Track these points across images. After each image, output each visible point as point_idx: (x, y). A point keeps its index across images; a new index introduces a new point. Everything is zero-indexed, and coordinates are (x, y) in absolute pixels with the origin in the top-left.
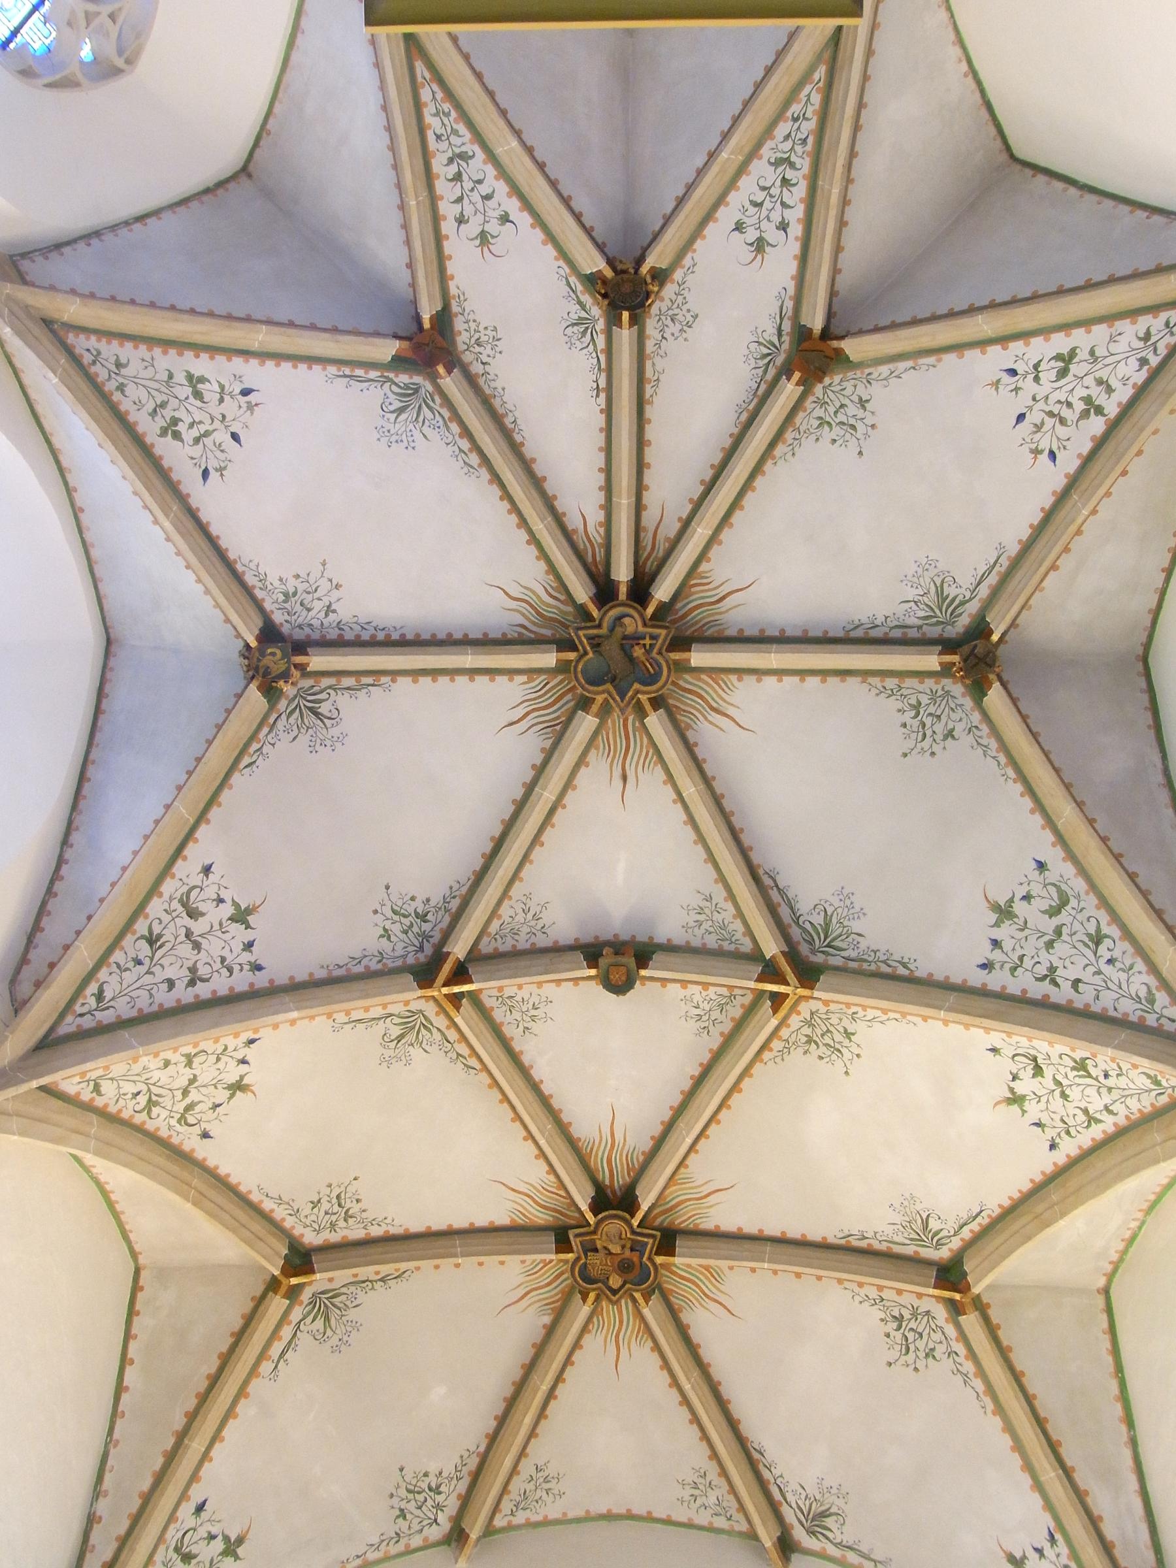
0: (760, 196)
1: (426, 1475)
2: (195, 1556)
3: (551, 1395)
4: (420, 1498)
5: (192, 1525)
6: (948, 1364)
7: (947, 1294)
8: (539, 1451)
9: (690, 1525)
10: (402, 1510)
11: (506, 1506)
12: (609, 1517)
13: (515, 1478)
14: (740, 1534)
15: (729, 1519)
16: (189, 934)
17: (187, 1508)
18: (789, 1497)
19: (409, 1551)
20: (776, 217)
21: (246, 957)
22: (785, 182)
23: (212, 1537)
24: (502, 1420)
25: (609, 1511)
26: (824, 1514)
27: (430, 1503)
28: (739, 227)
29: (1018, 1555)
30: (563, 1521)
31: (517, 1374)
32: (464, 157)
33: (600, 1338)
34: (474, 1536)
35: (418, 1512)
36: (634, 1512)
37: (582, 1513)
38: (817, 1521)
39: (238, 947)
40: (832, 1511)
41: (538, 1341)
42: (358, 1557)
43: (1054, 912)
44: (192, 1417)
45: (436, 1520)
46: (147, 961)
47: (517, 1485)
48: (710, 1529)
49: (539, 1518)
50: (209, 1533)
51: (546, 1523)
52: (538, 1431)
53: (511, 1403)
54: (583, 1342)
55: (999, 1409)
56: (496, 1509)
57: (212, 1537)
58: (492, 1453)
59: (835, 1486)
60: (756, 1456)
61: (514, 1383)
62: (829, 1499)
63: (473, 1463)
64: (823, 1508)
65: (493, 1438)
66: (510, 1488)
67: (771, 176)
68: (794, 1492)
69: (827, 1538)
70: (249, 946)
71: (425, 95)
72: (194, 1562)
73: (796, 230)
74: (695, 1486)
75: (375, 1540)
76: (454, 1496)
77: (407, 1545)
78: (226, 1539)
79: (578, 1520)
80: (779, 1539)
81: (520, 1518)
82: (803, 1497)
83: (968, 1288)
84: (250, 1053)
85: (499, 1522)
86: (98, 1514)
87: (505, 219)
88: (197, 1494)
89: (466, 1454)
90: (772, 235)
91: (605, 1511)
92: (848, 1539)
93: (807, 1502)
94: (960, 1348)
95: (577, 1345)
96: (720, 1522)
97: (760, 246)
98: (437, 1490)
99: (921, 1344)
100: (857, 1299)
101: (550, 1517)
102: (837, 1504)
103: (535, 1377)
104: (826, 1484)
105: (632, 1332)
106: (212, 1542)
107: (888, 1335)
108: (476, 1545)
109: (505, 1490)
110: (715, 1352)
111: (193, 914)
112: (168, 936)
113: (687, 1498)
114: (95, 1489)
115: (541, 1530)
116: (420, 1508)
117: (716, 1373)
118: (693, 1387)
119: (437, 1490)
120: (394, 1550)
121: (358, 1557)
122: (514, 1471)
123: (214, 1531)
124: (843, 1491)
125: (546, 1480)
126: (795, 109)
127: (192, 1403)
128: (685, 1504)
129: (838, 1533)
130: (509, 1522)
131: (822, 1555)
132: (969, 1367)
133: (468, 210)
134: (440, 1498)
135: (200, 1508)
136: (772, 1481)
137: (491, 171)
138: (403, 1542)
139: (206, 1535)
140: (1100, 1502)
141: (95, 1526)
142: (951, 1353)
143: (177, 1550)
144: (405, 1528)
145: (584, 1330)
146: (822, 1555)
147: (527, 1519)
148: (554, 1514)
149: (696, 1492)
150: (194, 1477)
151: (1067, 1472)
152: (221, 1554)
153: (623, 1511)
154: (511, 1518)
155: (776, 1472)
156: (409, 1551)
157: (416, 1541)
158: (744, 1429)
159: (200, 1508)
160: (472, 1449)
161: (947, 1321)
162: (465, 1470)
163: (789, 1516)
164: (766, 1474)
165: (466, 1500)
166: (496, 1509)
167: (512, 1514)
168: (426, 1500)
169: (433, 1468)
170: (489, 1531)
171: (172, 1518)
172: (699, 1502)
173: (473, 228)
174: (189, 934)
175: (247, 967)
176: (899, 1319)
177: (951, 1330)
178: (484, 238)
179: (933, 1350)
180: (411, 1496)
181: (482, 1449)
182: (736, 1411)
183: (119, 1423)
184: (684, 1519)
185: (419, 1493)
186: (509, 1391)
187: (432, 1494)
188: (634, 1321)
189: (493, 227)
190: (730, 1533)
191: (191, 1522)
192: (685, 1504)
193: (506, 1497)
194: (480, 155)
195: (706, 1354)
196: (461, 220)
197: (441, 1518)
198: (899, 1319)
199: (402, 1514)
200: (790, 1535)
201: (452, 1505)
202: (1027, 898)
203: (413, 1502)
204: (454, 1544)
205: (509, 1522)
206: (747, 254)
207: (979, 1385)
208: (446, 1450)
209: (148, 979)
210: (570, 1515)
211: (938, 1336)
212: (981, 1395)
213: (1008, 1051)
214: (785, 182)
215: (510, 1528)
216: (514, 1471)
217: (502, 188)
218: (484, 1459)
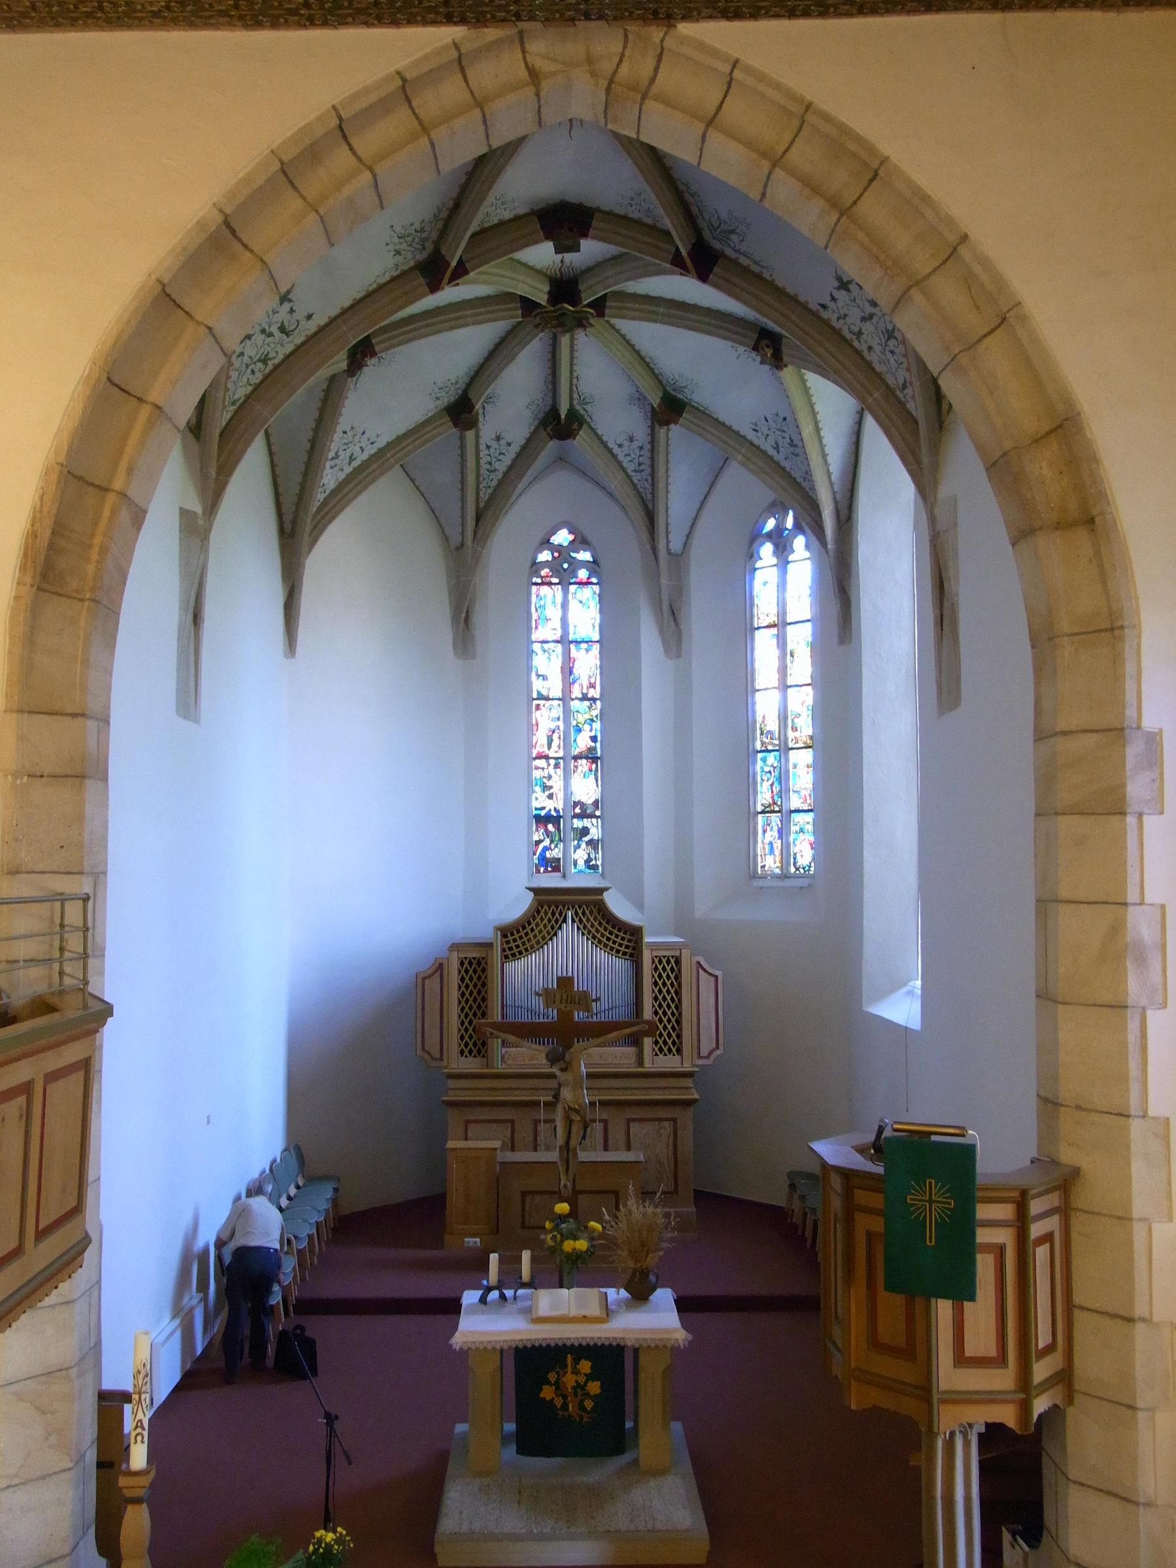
0: (501, 457)
20: (492, 450)
22: (490, 464)
28: (509, 444)
32: (635, 471)
43: (282, 329)
67: (497, 465)
71: (649, 496)
73: (482, 447)
84: (827, 300)
87: (620, 446)
90: (494, 444)
97: (498, 438)
126: (490, 491)
133: (637, 452)
137: (625, 465)
173: (635, 444)
178: (631, 439)
189: (626, 443)
194: (629, 471)
196: (641, 448)
202: (292, 311)
206: (503, 435)
213: (303, 323)
214: (490, 464)
217: (621, 458)
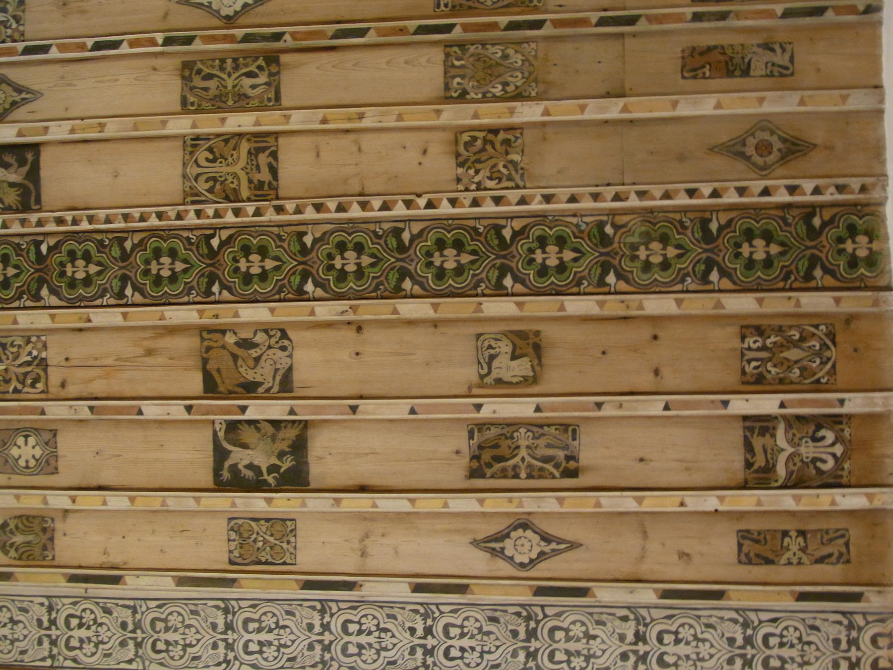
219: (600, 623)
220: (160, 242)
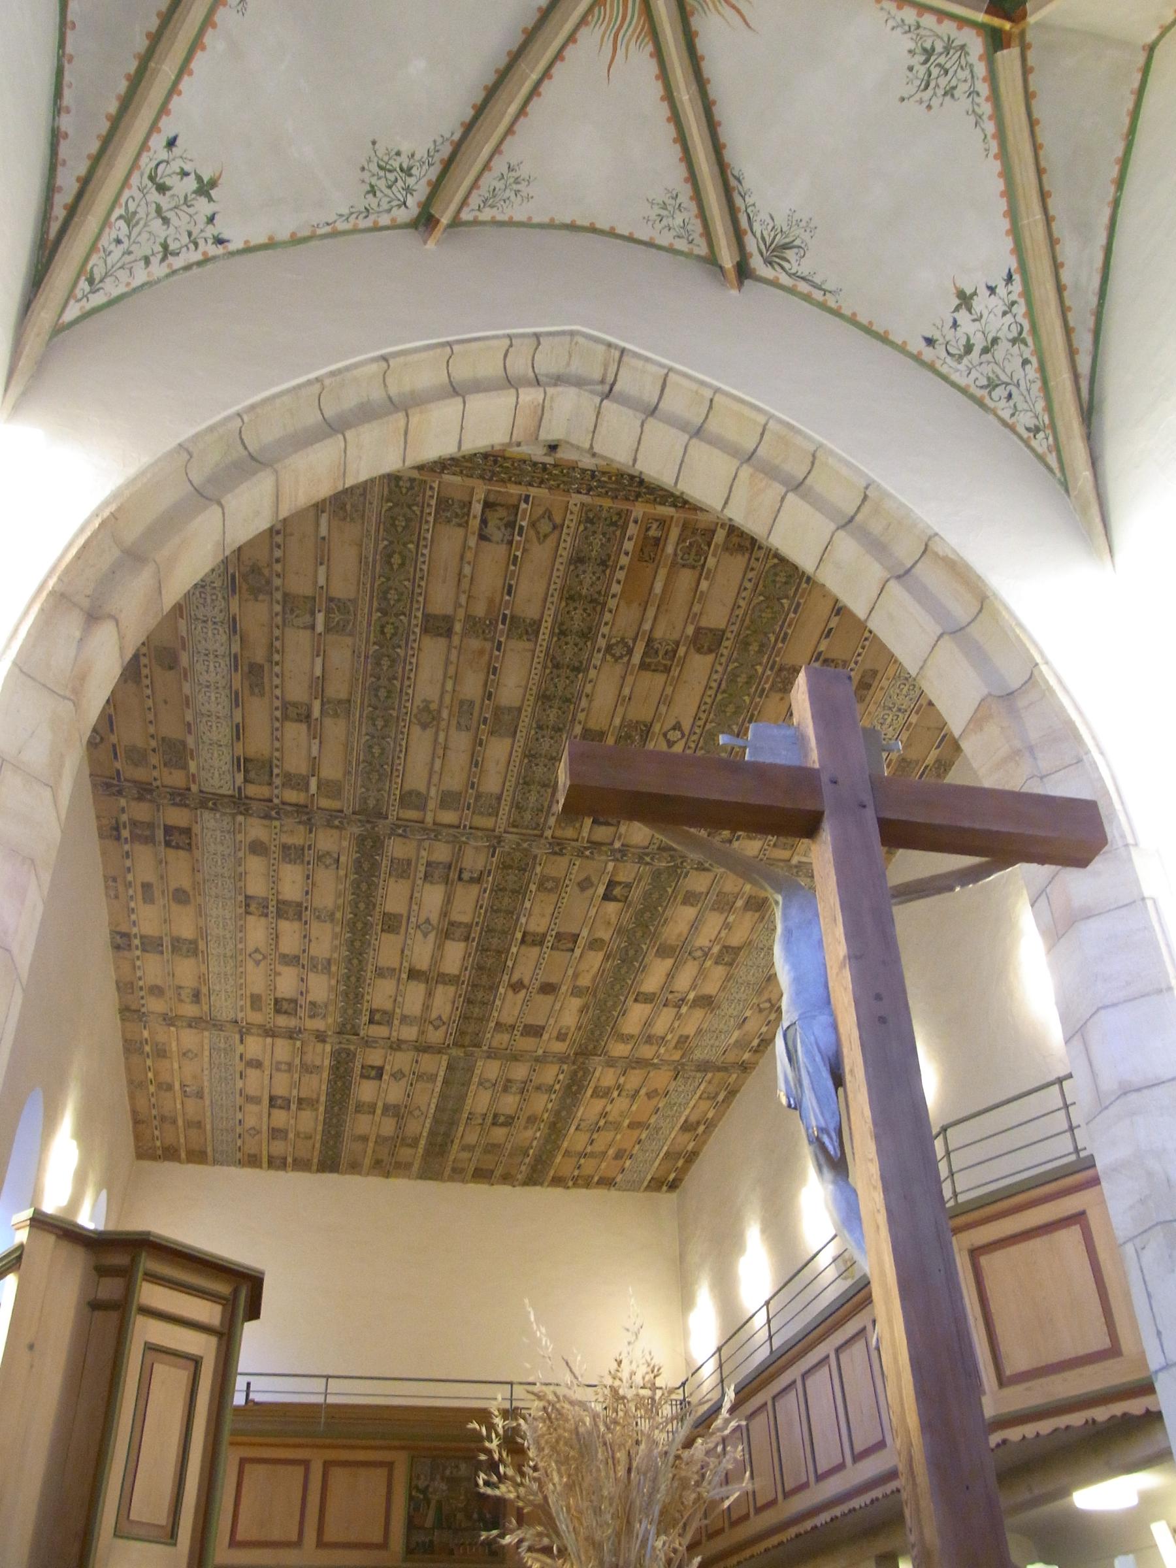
1: (398, 154)
2: (169, 189)
3: (535, 91)
4: (391, 176)
5: (166, 158)
6: (966, 103)
7: (997, 22)
8: (514, 150)
9: (650, 244)
10: (372, 186)
11: (474, 200)
12: (572, 227)
13: (486, 174)
14: (699, 258)
15: (691, 242)
16: (159, 210)
17: (158, 142)
18: (757, 227)
19: (377, 228)
21: (211, 231)
23: (185, 174)
24: (480, 110)
25: (573, 221)
26: (786, 247)
27: (400, 184)
29: (968, 292)
30: (527, 225)
31: (502, 62)
33: (598, 32)
34: (445, 221)
35: (388, 191)
36: (598, 226)
37: (546, 220)
38: (777, 252)
39: (201, 220)
40: (796, 243)
41: (530, 26)
42: (328, 224)
44: (155, 39)
45: (405, 203)
46: (125, 240)
47: (488, 181)
48: (670, 250)
49: (505, 218)
50: (182, 169)
51: (510, 223)
52: (516, 128)
53: (492, 92)
54: (578, 35)
55: (1004, 154)
56: (464, 202)
57: (185, 174)
58: (466, 143)
59: (805, 219)
60: (733, 182)
61: (497, 71)
62: (796, 231)
63: (446, 150)
64: (787, 240)
65: (469, 128)
66: (481, 183)
68: (762, 222)
69: (782, 268)
70: (211, 220)
72: (168, 193)
74: (664, 206)
75: (345, 211)
76: (424, 181)
77: (375, 222)
78: (199, 178)
79: (541, 226)
80: (738, 263)
81: (486, 215)
82: (770, 228)
83: (1024, 16)
85: (466, 216)
86: (63, 129)
88: (169, 126)
89: (440, 140)
91: (569, 222)
92: (804, 270)
93: (772, 234)
94: (984, 89)
95: (571, 38)
96: (681, 245)
98: (408, 172)
99: (943, 82)
100: (891, 23)
101: (515, 219)
102: (800, 235)
103: (522, 65)
104: (797, 216)
105: (635, 30)
106: (185, 179)
107: (911, 69)
108: (445, 230)
109: (475, 185)
110: (718, 68)
111: (162, 189)
112: (142, 213)
113: (653, 217)
114: (55, 103)
115: (505, 229)
116: (390, 187)
117: (713, 92)
118: (690, 99)
119: (408, 172)
120: (363, 224)
121: (328, 224)
122: (486, 167)
123: (187, 168)
124: (812, 225)
125: (517, 181)
127: (153, 24)
128: (650, 223)
129: (795, 264)
130: (476, 218)
131: (774, 283)
132: (987, 108)
134: (411, 181)
135: (171, 143)
136: (743, 208)
138: (372, 217)
139: (178, 170)
140: (1069, 250)
141: (62, 141)
142: (973, 93)
143: (152, 178)
144: (374, 206)
145: (583, 21)
146: (774, 283)
147: (493, 217)
148: (519, 217)
149: (664, 213)
150: (164, 110)
151: (1048, 220)
152: (195, 192)
153: (586, 223)
154: (478, 213)
155: (749, 200)
156: (377, 228)
157: (385, 220)
158: (728, 155)
159: (171, 143)
160: (447, 135)
161: (980, 58)
162: (437, 158)
163: (751, 244)
164: (738, 202)
165: (436, 187)
166: (464, 202)
167: (479, 210)
168: (396, 180)
169: (406, 148)
170: (456, 223)
171: (144, 146)
172: (664, 222)
174: (159, 210)
175: (210, 241)
176: (929, 53)
177: (981, 69)
179: (954, 88)
180: (382, 173)
181: (456, 137)
182: (724, 135)
183: (70, 36)
184: (645, 238)
185: (390, 171)
186: (490, 79)
187: (403, 175)
188: (639, 18)
190: (688, 255)
191: (163, 154)
192: (650, 223)
193: (475, 192)
195: (708, 69)
197: (410, 201)
198: (929, 53)
199: (373, 191)
200: (747, 264)
201: (422, 191)
203: (383, 180)
204: (421, 229)
205: (476, 218)
207: (990, 127)
208: (421, 137)
209: (127, 258)
210: (536, 220)
211: (965, 74)
212: (989, 137)
215: (475, 223)
216: (486, 167)
218: (457, 147)
219: (221, 611)
220: (358, 997)
